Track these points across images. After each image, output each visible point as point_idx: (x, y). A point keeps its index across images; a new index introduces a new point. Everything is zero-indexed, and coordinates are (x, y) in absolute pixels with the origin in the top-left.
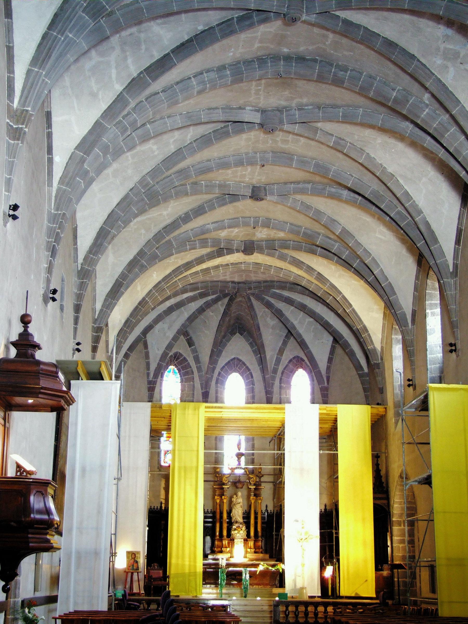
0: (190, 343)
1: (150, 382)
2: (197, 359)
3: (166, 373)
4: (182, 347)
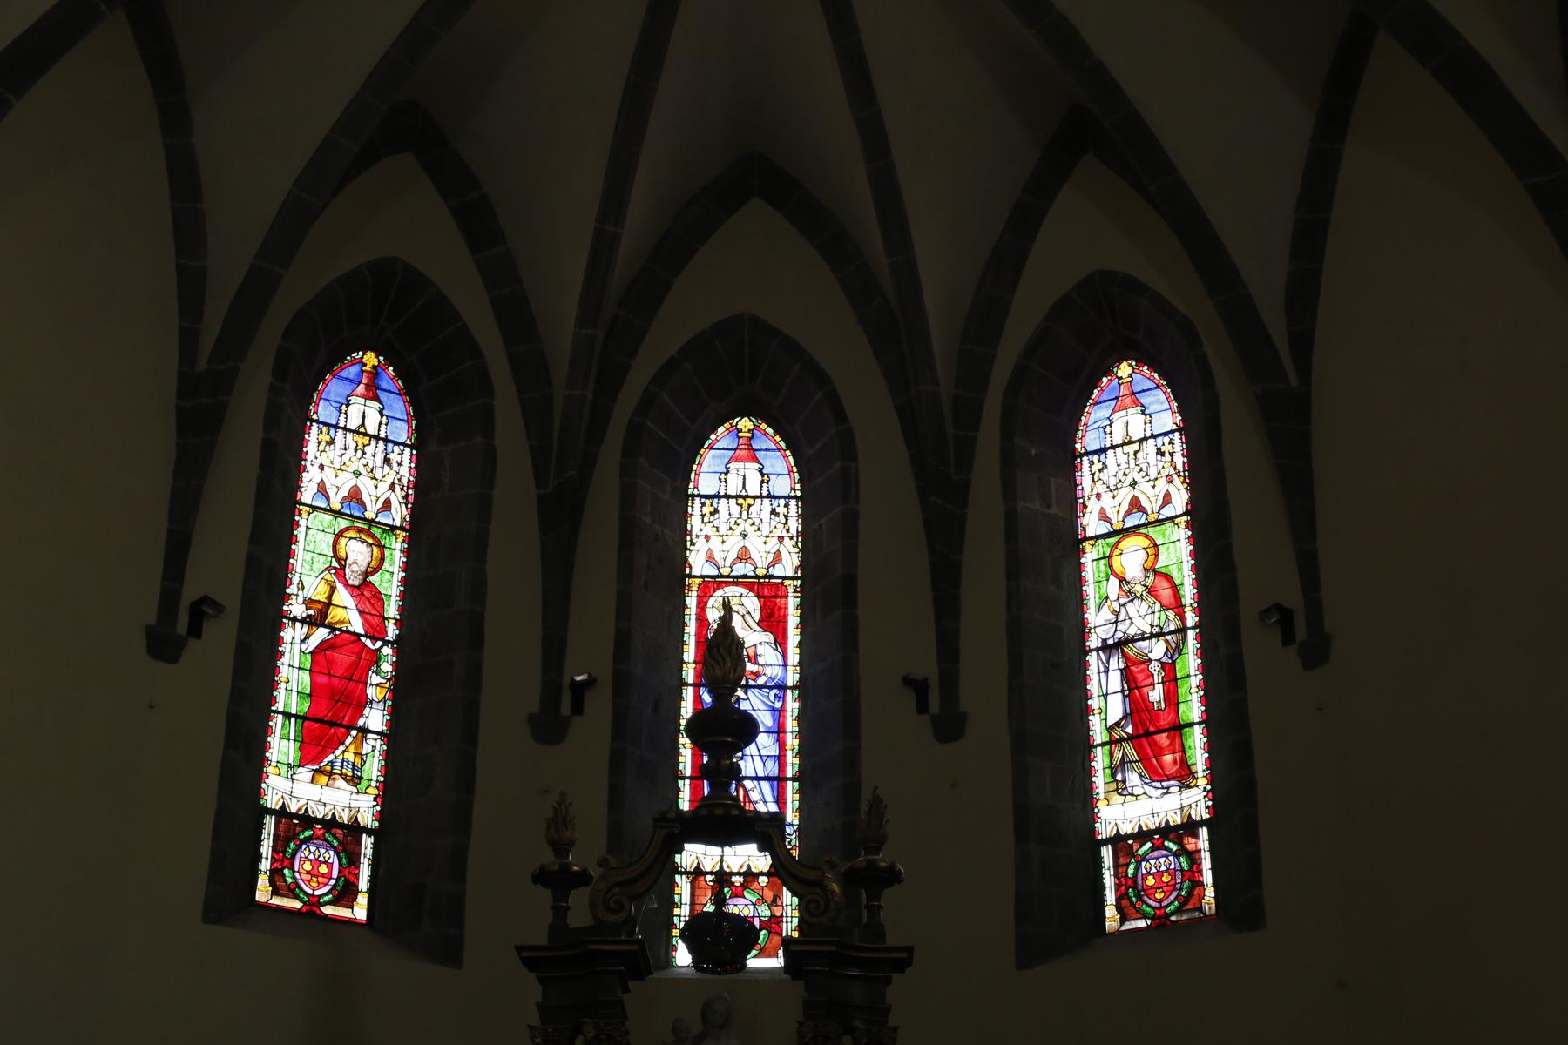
0: (479, 225)
1: (189, 384)
2: (516, 316)
3: (334, 388)
4: (404, 223)
